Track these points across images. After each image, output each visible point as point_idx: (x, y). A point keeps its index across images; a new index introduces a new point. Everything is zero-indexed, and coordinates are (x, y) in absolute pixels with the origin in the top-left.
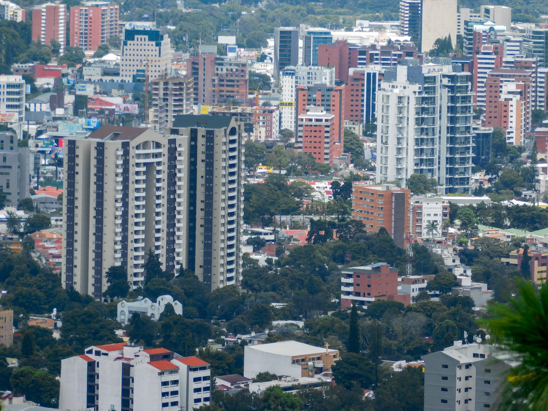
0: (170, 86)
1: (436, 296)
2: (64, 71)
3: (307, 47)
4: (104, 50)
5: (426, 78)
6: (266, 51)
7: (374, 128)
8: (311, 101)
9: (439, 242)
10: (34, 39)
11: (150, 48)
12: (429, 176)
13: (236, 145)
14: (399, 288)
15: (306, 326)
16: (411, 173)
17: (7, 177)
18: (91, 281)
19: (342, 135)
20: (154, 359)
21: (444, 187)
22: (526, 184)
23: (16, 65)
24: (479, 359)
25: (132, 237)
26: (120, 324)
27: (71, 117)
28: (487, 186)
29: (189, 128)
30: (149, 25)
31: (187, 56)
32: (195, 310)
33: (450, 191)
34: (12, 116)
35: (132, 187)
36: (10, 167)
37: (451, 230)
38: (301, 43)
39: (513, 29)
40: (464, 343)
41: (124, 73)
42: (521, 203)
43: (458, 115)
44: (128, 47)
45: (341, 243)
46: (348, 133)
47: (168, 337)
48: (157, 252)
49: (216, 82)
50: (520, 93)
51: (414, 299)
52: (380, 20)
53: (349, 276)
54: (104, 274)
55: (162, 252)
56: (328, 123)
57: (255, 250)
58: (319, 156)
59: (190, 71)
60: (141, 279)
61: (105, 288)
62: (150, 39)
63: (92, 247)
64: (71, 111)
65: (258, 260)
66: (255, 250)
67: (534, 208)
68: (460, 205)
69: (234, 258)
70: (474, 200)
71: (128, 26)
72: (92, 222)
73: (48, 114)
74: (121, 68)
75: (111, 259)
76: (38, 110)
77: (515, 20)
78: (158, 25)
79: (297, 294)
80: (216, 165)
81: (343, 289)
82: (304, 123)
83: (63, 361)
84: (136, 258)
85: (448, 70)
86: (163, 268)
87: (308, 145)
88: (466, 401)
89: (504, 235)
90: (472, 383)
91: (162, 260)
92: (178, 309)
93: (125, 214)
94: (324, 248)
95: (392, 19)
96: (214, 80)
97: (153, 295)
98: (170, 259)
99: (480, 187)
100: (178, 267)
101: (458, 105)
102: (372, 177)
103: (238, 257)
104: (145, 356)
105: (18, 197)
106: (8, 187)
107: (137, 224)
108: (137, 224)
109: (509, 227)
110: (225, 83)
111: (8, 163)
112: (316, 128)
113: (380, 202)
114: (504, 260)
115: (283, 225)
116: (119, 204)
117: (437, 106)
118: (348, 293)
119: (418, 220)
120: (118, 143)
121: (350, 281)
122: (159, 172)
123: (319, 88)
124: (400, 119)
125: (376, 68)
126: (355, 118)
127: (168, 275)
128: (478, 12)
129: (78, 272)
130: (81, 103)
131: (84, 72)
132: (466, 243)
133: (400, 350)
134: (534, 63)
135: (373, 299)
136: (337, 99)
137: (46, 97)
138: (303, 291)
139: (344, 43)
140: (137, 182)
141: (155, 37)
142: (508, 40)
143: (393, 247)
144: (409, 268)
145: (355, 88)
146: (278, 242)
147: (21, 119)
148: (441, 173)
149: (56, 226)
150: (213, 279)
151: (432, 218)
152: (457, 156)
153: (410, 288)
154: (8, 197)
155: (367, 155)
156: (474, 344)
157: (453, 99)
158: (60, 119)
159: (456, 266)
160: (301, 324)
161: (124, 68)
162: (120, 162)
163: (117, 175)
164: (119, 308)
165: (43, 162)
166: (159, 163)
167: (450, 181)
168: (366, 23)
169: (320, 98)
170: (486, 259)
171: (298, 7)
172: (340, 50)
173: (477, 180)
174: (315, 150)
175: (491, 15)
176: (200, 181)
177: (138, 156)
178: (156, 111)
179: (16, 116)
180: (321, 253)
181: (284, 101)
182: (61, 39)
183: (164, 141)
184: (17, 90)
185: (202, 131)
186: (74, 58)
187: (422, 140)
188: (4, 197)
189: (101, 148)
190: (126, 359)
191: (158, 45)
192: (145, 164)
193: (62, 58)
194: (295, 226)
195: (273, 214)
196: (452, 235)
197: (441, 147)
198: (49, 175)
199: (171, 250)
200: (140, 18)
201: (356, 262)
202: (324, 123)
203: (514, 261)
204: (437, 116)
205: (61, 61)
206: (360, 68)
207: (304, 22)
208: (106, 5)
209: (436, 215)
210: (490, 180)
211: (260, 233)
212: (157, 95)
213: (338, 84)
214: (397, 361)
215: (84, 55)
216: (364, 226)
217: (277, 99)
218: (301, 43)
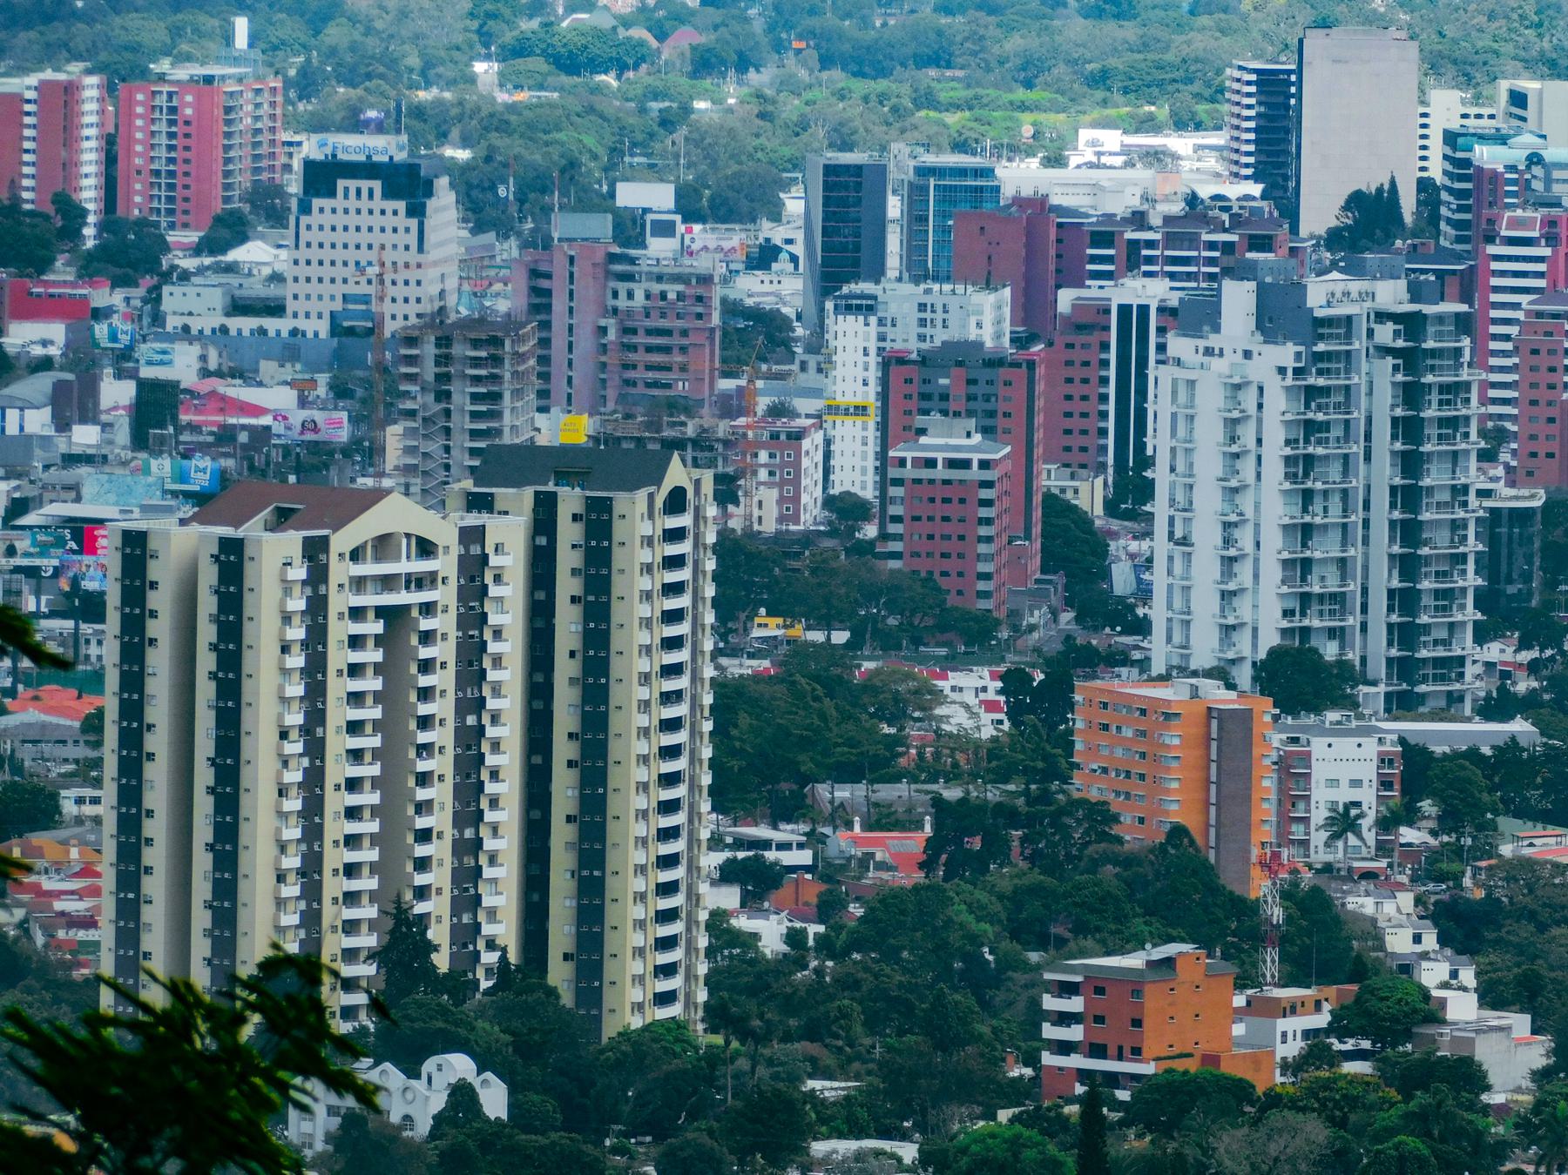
0: (460, 350)
3: (915, 219)
4: (229, 230)
6: (777, 234)
7: (1146, 491)
8: (933, 401)
9: (1368, 875)
12: (1330, 650)
15: (925, 1159)
16: (1270, 639)
19: (1037, 514)
21: (1382, 688)
25: (335, 857)
29: (528, 493)
30: (387, 147)
37: (1408, 835)
43: (1427, 448)
44: (315, 219)
45: (1037, 877)
46: (1057, 507)
48: (420, 908)
49: (612, 335)
51: (1285, 1066)
53: (1067, 989)
55: (437, 909)
57: (751, 902)
64: (123, 435)
65: (756, 936)
66: (751, 902)
68: (1439, 749)
71: (311, 147)
73: (45, 440)
75: (267, 927)
79: (889, 1049)
81: (1049, 1031)
82: (909, 472)
86: (441, 961)
91: (439, 933)
92: (494, 1100)
94: (981, 896)
98: (466, 935)
99: (1502, 689)
100: (489, 958)
102: (1137, 655)
103: (691, 922)
110: (641, 339)
115: (840, 816)
116: (295, 747)
118: (1065, 1048)
120: (291, 541)
121: (1075, 1004)
126: (1077, 457)
127: (459, 983)
130: (156, 408)
131: (167, 304)
132: (1457, 877)
135: (1148, 1069)
138: (910, 1038)
145: (1078, 355)
146: (826, 871)
149: (79, 821)
151: (1344, 795)
153: (1276, 1031)
155: (1122, 579)
158: (87, 459)
159: (1425, 956)
160: (908, 1152)
161: (301, 289)
166: (428, 609)
173: (1489, 666)
174: (947, 565)
175: (1531, 113)
177: (359, 583)
180: (970, 911)
181: (841, 400)
182: (89, 194)
185: (570, 500)
191: (416, 211)
192: (381, 612)
193: (91, 256)
194: (882, 819)
195: (806, 779)
199: (467, 901)
201: (1089, 943)
202: (974, 474)
206: (1094, 290)
209: (1356, 783)
210: (1533, 668)
211: (766, 844)
215: (166, 248)
216: (1115, 819)
217: (817, 393)
218: (894, 207)
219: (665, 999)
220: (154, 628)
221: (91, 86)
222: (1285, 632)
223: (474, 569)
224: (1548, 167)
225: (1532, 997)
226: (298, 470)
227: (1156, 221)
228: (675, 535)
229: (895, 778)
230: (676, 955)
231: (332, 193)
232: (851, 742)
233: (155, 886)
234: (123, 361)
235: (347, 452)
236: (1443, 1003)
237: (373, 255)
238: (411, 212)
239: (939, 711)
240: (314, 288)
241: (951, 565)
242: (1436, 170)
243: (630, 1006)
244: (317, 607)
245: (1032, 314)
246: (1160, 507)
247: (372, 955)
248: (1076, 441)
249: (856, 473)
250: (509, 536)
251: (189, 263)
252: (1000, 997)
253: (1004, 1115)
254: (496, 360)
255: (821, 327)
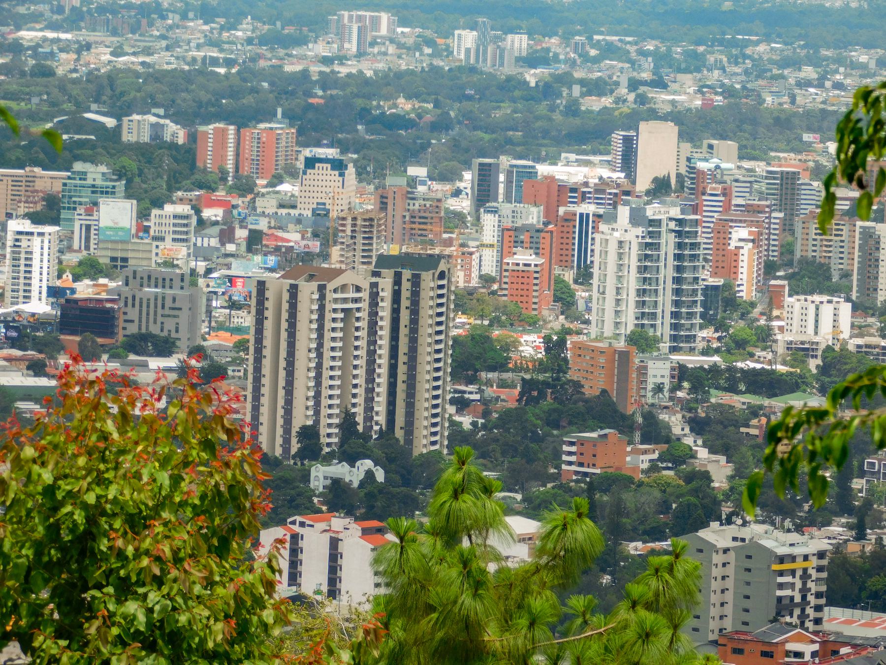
0: (359, 222)
1: (668, 468)
2: (234, 202)
3: (509, 182)
4: (277, 180)
5: (651, 221)
6: (462, 185)
7: (591, 276)
8: (517, 243)
9: (666, 407)
10: (200, 164)
11: (333, 178)
12: (651, 332)
13: (444, 291)
14: (628, 459)
15: (524, 500)
16: (630, 328)
17: (176, 320)
18: (279, 441)
19: (552, 282)
20: (366, 532)
21: (668, 344)
22: (759, 344)
23: (180, 193)
24: (739, 544)
25: (325, 392)
26: (313, 491)
27: (245, 254)
28: (715, 345)
29: (393, 271)
30: (331, 153)
31: (371, 188)
32: (397, 478)
33: (674, 350)
34: (180, 250)
35: (328, 335)
36: (180, 309)
37: (680, 394)
38: (502, 178)
39: (739, 167)
40: (721, 524)
41: (302, 206)
42: (758, 366)
43: (686, 264)
44: (308, 176)
45: (556, 405)
46: (559, 281)
47: (371, 507)
48: (353, 410)
49: (407, 218)
50: (753, 241)
51: (643, 471)
52: (587, 154)
53: (572, 444)
54: (294, 433)
55: (359, 411)
56: (538, 269)
57: (459, 411)
58: (526, 305)
59: (378, 207)
60: (335, 440)
61: (294, 450)
62: (333, 169)
63: (281, 402)
64: (243, 247)
65: (461, 423)
66: (459, 411)
67: (773, 372)
68: (690, 366)
69: (438, 420)
70: (708, 361)
71: (307, 152)
72: (282, 374)
73: (217, 249)
74: (299, 200)
75: (301, 418)
76: (206, 245)
77: (741, 158)
78: (342, 153)
79: (510, 462)
80: (422, 313)
81: (565, 458)
82: (511, 267)
83: (262, 532)
84: (330, 416)
85: (675, 212)
86: (360, 428)
87: (515, 292)
88: (723, 591)
89: (739, 401)
90: (730, 570)
91: (360, 419)
92: (380, 475)
93: (319, 366)
94: (537, 411)
95: (601, 154)
96: (404, 217)
97: (352, 459)
98: (368, 418)
99: (708, 346)
100: (376, 428)
101: (686, 252)
102: (585, 331)
103: (443, 418)
104: (356, 529)
105: (188, 343)
106: (177, 331)
107: (332, 378)
108: (332, 378)
109: (744, 393)
110: (417, 220)
111: (177, 305)
112: (524, 274)
113: (602, 360)
114: (743, 430)
115: (489, 383)
116: (313, 355)
117: (662, 253)
118: (570, 463)
119: (642, 381)
120: (314, 285)
121: (573, 449)
122: (358, 319)
123: (526, 229)
124: (620, 267)
125: (588, 208)
126: (563, 264)
127: (366, 436)
128: (700, 147)
129: (264, 430)
130: (255, 240)
131: (257, 204)
132: (696, 409)
133: (635, 529)
134: (768, 206)
135: (598, 471)
136: (547, 241)
137: (216, 230)
138: (517, 459)
139: (551, 179)
140: (334, 330)
141: (339, 166)
142: (736, 181)
143: (616, 411)
144: (637, 436)
145: (565, 229)
146: (484, 402)
147: (189, 255)
148: (663, 329)
149: (233, 377)
150: (415, 442)
151: (659, 380)
152: (683, 310)
153: (639, 459)
154: (178, 343)
155: (581, 305)
156: (733, 526)
157: (680, 246)
158: (232, 255)
159: (685, 435)
160: (519, 497)
161: (303, 200)
162: (315, 307)
163: (311, 322)
164: (313, 473)
165: (214, 304)
166: (358, 310)
167: (674, 338)
168: (573, 157)
169: (529, 240)
170: (719, 428)
171: (494, 136)
172: (549, 187)
173: (704, 338)
174: (522, 299)
175: (714, 151)
176: (403, 331)
177: (336, 301)
178: (342, 249)
179: (184, 251)
180: (533, 415)
181: (485, 242)
182: (230, 166)
183: (365, 285)
184: (185, 222)
185: (407, 274)
186: (245, 187)
187: (644, 290)
188: (174, 343)
189: (294, 291)
190: (334, 532)
191: (342, 175)
192: (343, 310)
193: (231, 187)
194: (503, 384)
195: (476, 371)
196: (680, 400)
197: (665, 300)
198: (221, 319)
199: (369, 409)
200: (318, 144)
201: (574, 428)
202: (532, 268)
203: (754, 432)
204: (662, 264)
205: (230, 191)
206: (572, 208)
207: (503, 153)
208: (282, 129)
209: (663, 376)
210: (719, 339)
211: (464, 392)
212: (344, 231)
213: (546, 224)
214: (632, 541)
215: (256, 185)
216: (583, 386)
217: (476, 240)
218: (502, 178)
219: (434, 443)
220: (267, 314)
221: (232, 129)
222: (636, 325)
223: (374, 297)
224: (722, 170)
225: (727, 450)
226: (302, 261)
227: (592, 185)
228: (441, 287)
229: (507, 371)
230: (438, 429)
231: (314, 168)
232: (493, 359)
233: (265, 401)
234: (243, 224)
235: (318, 255)
236: (696, 451)
237: (331, 190)
238: (340, 175)
239: (521, 348)
240: (307, 200)
241: (524, 299)
242: (683, 170)
243: (422, 446)
244: (322, 309)
245: (550, 216)
246: (595, 281)
247: (337, 426)
248: (564, 258)
249: (490, 267)
250: (386, 284)
251: (264, 190)
252: (543, 445)
253: (549, 486)
254: (371, 226)
255: (478, 219)
